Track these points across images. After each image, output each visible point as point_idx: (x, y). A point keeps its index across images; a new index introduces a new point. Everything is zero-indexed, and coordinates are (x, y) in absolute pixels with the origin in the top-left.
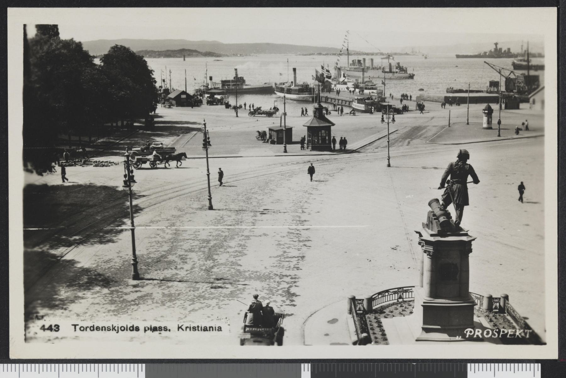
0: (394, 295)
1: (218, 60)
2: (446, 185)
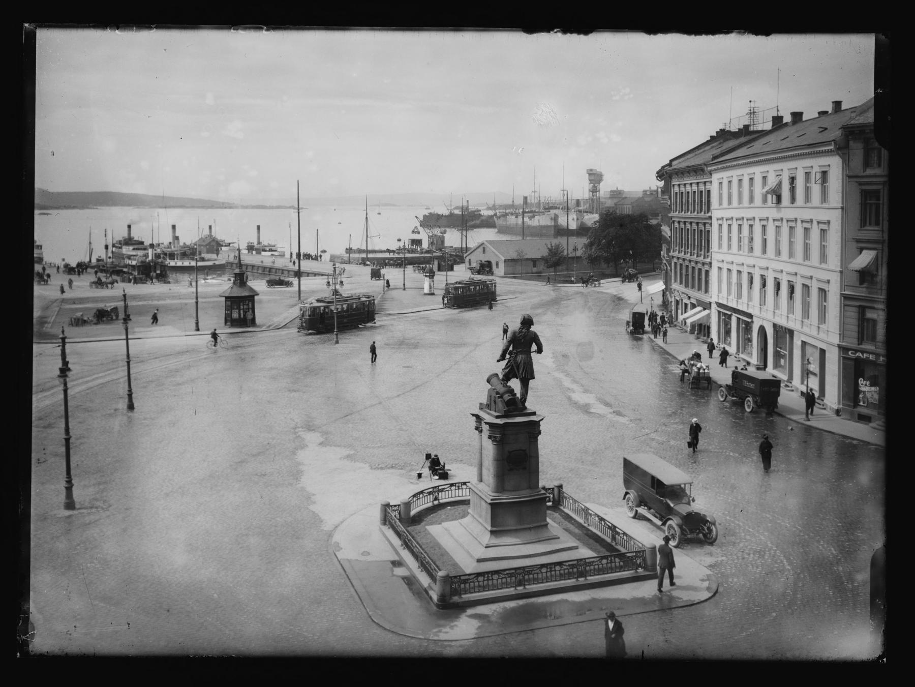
0: (429, 496)
1: (44, 214)
2: (508, 356)
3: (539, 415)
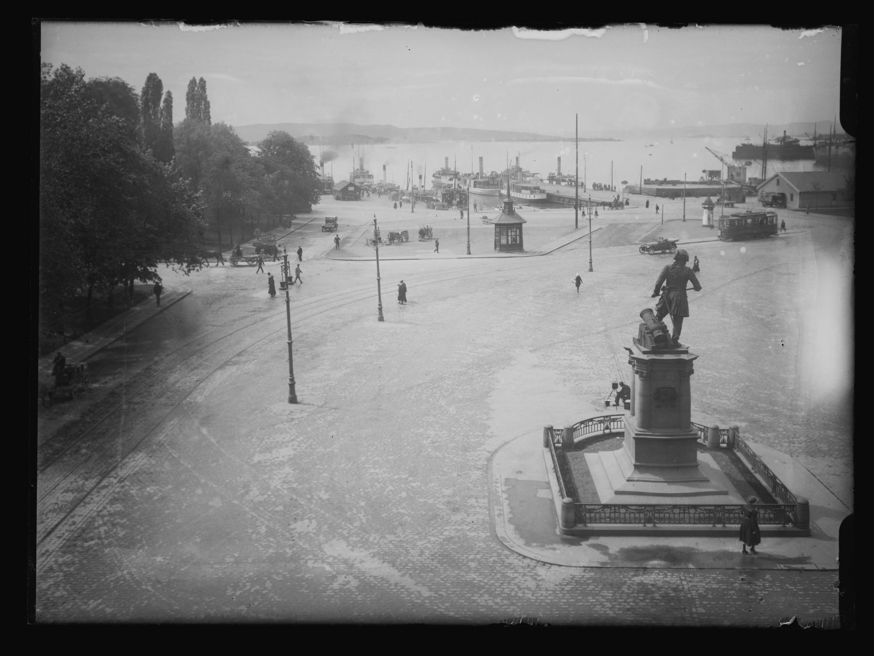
0: (599, 425)
2: (661, 292)
3: (692, 354)
